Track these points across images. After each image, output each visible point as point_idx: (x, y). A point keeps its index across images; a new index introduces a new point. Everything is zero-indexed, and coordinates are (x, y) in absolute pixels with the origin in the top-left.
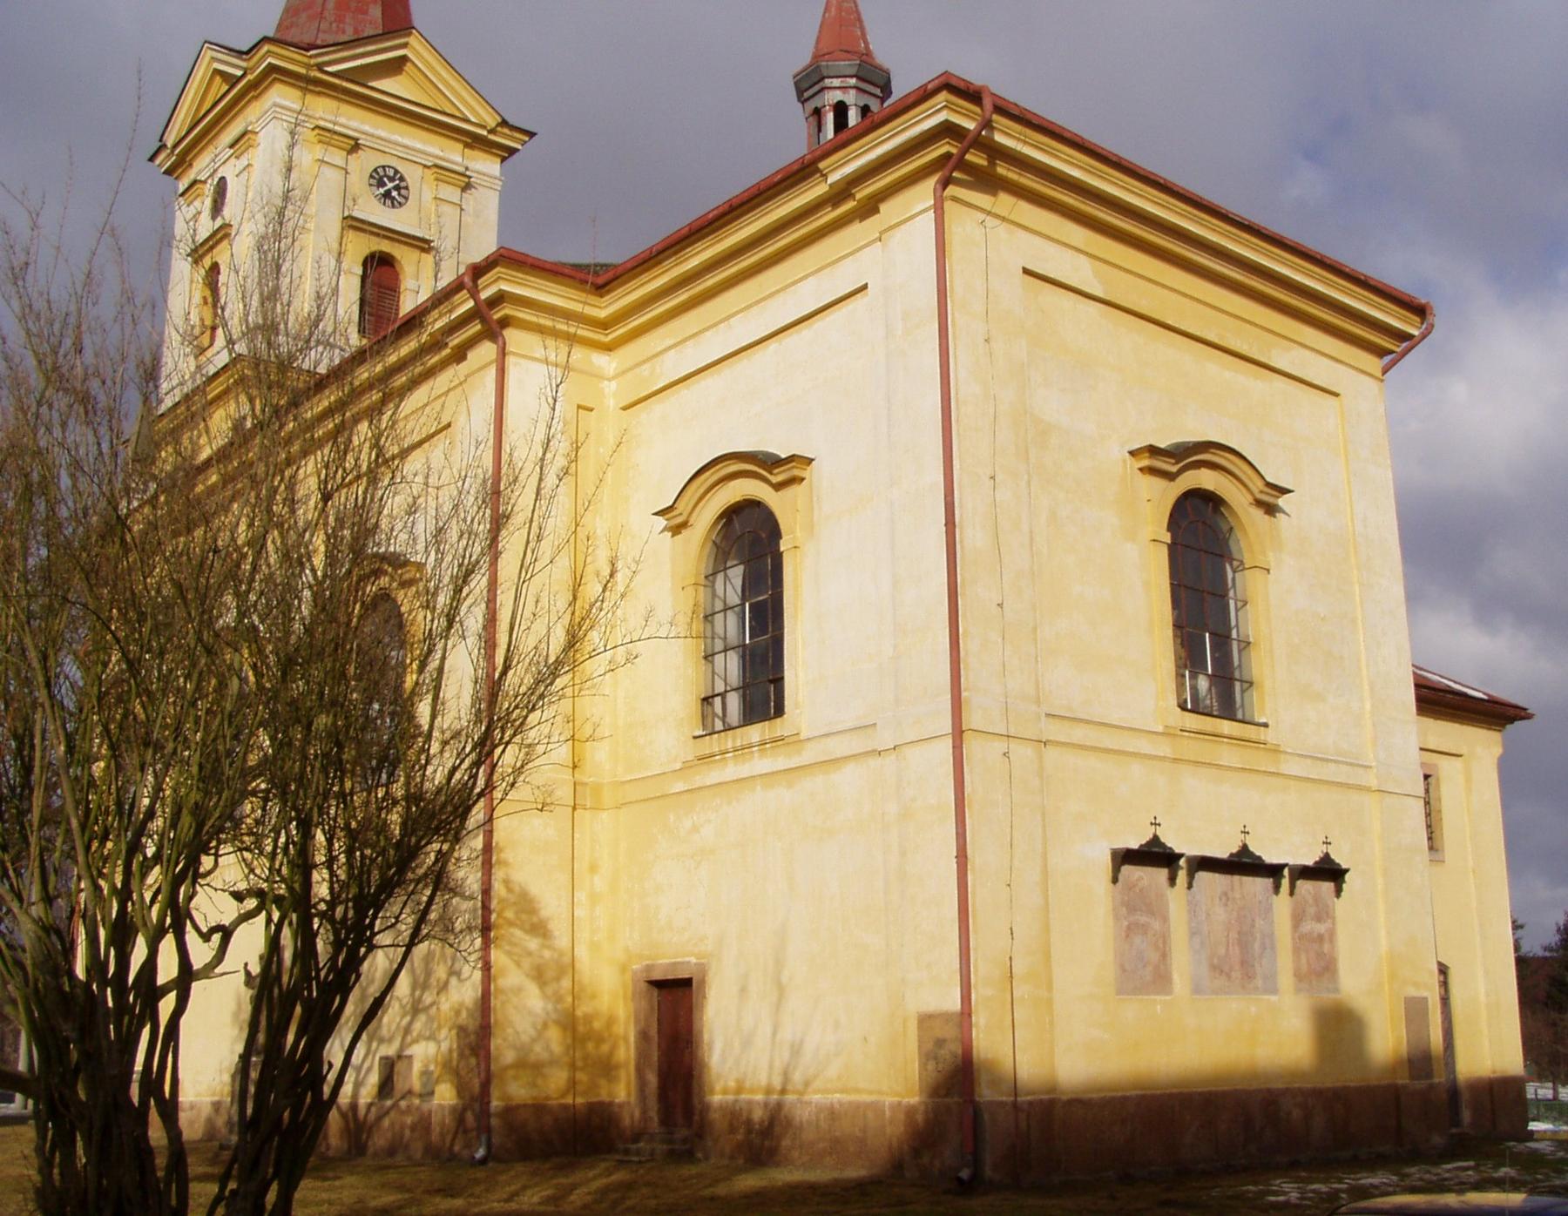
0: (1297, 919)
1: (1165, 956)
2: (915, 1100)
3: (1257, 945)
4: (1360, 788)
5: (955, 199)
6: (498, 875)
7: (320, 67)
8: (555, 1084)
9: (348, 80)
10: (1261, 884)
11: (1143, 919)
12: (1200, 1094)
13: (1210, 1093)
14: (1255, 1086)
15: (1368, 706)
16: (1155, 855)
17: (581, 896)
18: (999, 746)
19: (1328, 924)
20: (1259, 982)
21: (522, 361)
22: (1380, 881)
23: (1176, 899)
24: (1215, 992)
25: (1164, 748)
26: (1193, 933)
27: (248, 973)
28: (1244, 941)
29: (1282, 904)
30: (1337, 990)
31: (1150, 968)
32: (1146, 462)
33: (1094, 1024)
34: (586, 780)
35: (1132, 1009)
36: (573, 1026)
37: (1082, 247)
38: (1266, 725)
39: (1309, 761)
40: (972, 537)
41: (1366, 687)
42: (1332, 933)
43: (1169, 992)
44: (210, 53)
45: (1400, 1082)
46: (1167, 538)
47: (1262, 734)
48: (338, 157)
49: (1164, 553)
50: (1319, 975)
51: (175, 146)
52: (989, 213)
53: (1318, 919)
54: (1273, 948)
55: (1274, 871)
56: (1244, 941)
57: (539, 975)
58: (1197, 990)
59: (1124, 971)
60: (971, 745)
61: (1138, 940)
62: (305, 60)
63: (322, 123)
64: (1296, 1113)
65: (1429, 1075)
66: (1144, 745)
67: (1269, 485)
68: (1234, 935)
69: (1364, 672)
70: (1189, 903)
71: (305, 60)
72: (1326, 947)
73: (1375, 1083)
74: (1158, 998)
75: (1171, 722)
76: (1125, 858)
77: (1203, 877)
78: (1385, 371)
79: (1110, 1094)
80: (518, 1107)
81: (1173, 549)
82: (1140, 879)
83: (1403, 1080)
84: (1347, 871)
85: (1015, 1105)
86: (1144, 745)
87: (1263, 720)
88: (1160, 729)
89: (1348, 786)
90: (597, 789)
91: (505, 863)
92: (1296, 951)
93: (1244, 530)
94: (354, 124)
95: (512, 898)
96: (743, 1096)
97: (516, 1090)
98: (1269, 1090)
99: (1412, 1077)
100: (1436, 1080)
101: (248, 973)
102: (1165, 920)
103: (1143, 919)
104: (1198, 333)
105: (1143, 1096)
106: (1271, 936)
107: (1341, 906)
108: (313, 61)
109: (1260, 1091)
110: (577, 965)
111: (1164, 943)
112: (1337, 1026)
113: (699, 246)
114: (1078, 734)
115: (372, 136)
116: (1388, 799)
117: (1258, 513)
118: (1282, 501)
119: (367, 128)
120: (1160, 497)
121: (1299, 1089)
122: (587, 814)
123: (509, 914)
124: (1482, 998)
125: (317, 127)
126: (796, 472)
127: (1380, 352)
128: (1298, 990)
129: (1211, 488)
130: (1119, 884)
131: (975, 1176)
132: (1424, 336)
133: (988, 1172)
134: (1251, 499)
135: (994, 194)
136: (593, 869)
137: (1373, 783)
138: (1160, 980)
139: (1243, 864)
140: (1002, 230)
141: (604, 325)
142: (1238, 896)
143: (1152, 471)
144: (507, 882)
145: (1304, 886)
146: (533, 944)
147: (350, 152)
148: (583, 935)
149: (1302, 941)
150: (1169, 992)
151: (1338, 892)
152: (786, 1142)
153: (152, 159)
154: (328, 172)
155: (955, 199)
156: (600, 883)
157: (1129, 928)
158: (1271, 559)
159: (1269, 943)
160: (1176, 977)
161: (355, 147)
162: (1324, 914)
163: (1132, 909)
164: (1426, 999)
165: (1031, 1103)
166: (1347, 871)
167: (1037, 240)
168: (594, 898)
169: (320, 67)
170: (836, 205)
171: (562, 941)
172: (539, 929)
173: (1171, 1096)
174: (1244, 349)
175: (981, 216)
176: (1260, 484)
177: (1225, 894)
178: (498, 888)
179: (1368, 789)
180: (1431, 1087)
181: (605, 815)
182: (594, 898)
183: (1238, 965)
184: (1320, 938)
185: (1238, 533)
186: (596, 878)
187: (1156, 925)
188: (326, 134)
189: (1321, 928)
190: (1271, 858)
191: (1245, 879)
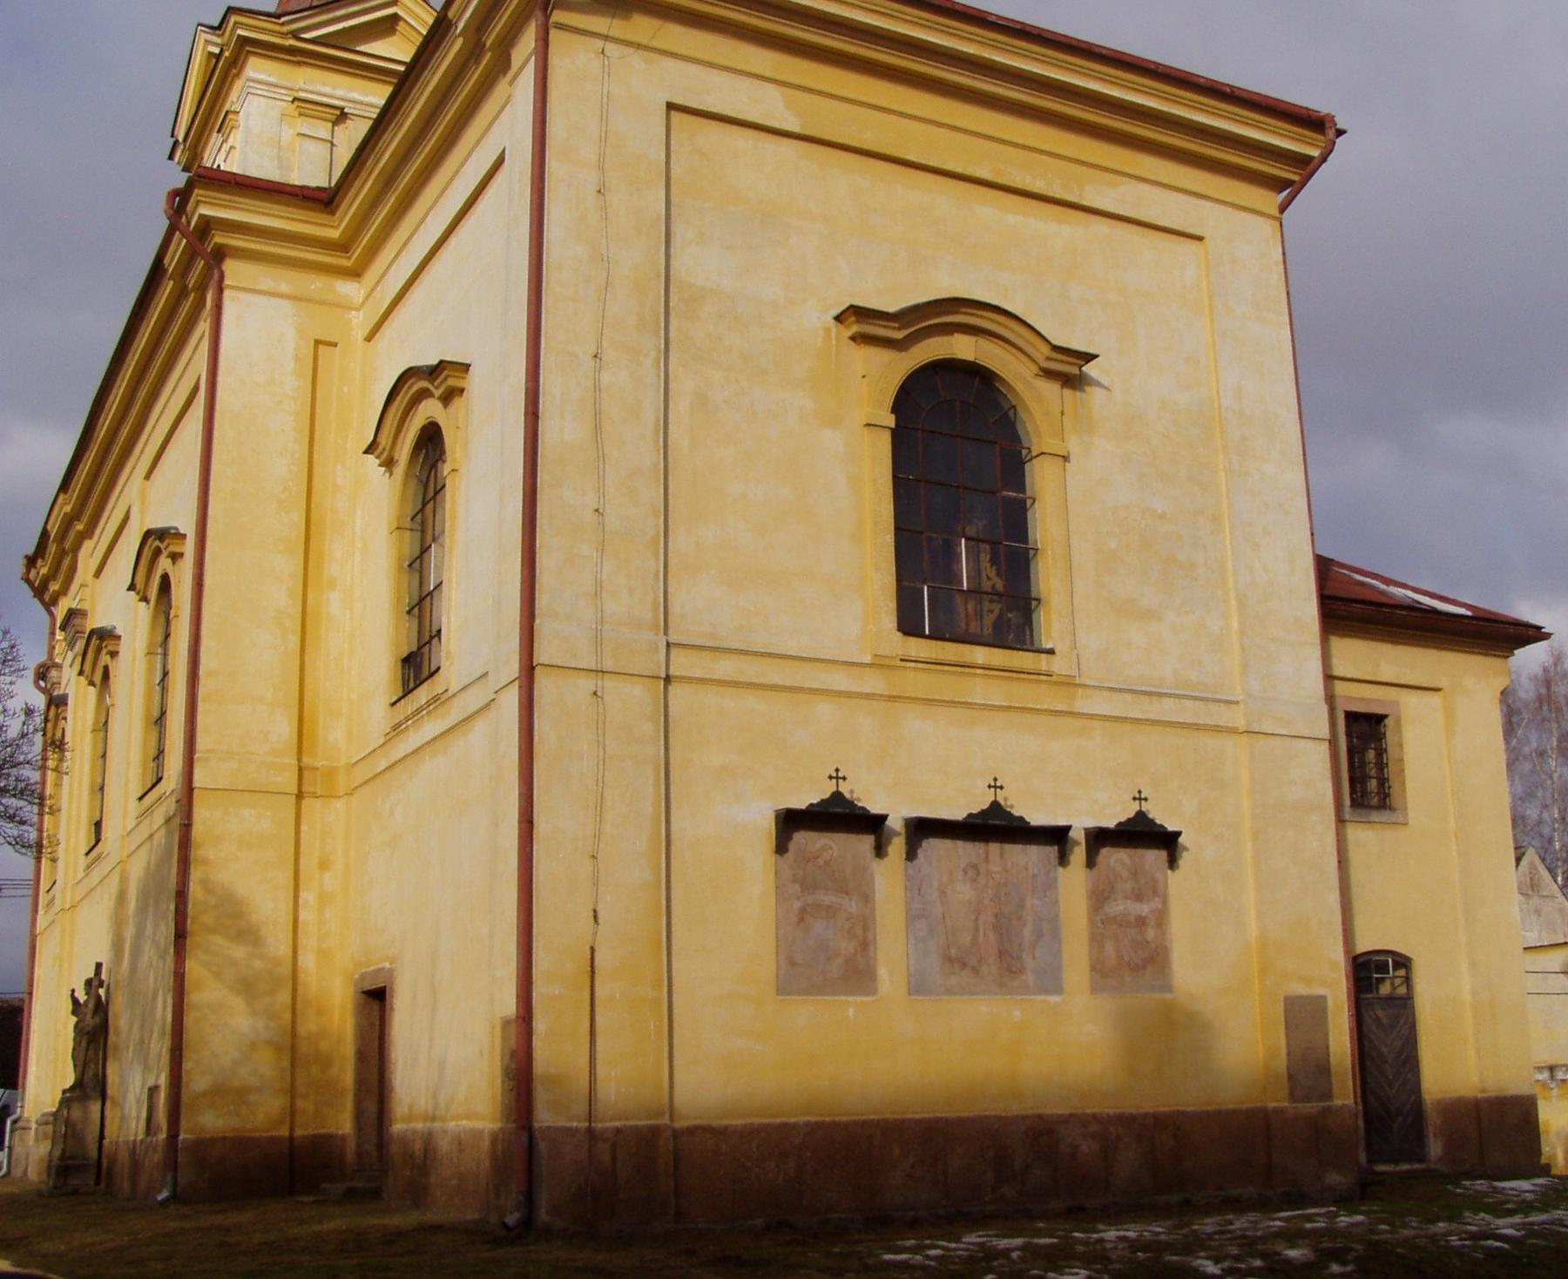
0: (1099, 898)
1: (865, 945)
2: (497, 1125)
3: (1027, 933)
4: (1217, 729)
5: (561, 27)
6: (196, 874)
7: (295, 35)
8: (263, 1115)
9: (327, 46)
10: (1033, 856)
11: (828, 899)
12: (919, 1122)
13: (937, 1120)
14: (1016, 1109)
15: (1235, 624)
16: (839, 815)
17: (307, 896)
18: (587, 684)
19: (1156, 903)
20: (1030, 978)
21: (242, 295)
22: (1248, 847)
23: (888, 877)
24: (949, 992)
25: (874, 683)
26: (913, 917)
27: (75, 1001)
28: (1004, 927)
29: (1074, 881)
30: (1168, 988)
31: (839, 961)
32: (855, 329)
33: (736, 1030)
34: (319, 764)
35: (804, 1014)
36: (293, 1049)
37: (768, 74)
38: (1051, 652)
39: (1128, 697)
40: (557, 429)
41: (1233, 602)
42: (1161, 918)
43: (873, 992)
44: (204, 36)
45: (1272, 1105)
46: (891, 421)
47: (1043, 662)
48: (323, 130)
49: (885, 441)
50: (1137, 969)
51: (185, 140)
52: (606, 38)
53: (1138, 897)
54: (1056, 934)
55: (1057, 836)
56: (1004, 927)
57: (247, 987)
58: (918, 986)
59: (792, 963)
60: (545, 684)
61: (819, 926)
62: (277, 28)
63: (302, 95)
64: (1087, 1147)
65: (1328, 1095)
66: (839, 680)
67: (1056, 349)
68: (987, 918)
69: (1231, 584)
70: (908, 877)
71: (277, 28)
72: (1151, 933)
73: (1231, 1107)
74: (850, 999)
75: (885, 650)
76: (790, 822)
77: (934, 848)
78: (1283, 208)
79: (758, 1121)
80: (213, 1141)
81: (900, 438)
82: (823, 849)
83: (1278, 1100)
84: (1178, 834)
85: (591, 1133)
86: (839, 680)
87: (1049, 646)
88: (868, 659)
89: (1197, 727)
90: (330, 773)
91: (205, 862)
92: (1096, 939)
93: (1027, 409)
94: (340, 93)
95: (212, 901)
96: (437, 1125)
97: (208, 1121)
98: (1040, 1116)
99: (1292, 1097)
100: (1338, 1102)
101: (75, 1001)
102: (867, 898)
103: (828, 899)
104: (959, 170)
105: (820, 1125)
106: (1054, 920)
107: (1177, 882)
108: (285, 29)
109: (1024, 1117)
110: (301, 976)
111: (865, 929)
112: (1168, 1030)
113: (387, 136)
114: (726, 667)
115: (361, 103)
116: (1262, 742)
117: (1050, 389)
118: (1090, 369)
119: (355, 96)
120: (884, 372)
121: (1094, 1116)
122: (319, 802)
123: (208, 919)
124: (1467, 997)
125: (295, 99)
126: (451, 382)
127: (1278, 185)
128: (1095, 989)
129: (970, 357)
130: (790, 856)
131: (528, 1221)
132: (1324, 159)
133: (543, 1215)
134: (1035, 370)
135: (627, 18)
136: (324, 865)
137: (1241, 723)
138: (857, 975)
139: (994, 826)
140: (636, 59)
141: (343, 247)
142: (995, 868)
143: (861, 339)
144: (206, 884)
145: (1115, 858)
146: (239, 952)
147: (335, 123)
148: (308, 943)
149: (1102, 926)
150: (873, 992)
151: (1172, 862)
152: (433, 1180)
153: (171, 157)
154: (311, 146)
155: (561, 27)
156: (330, 881)
157: (803, 910)
158: (1073, 445)
159: (1050, 928)
160: (882, 972)
161: (342, 116)
162: (1149, 890)
163: (808, 886)
164: (1323, 998)
165: (618, 1131)
166: (1178, 834)
167: (693, 69)
168: (324, 899)
169: (295, 35)
170: (477, 62)
171: (278, 945)
172: (248, 934)
173: (865, 1124)
174: (1039, 186)
175: (600, 43)
176: (1045, 350)
177: (975, 867)
178: (195, 890)
179: (1233, 731)
180: (1328, 1110)
181: (339, 805)
182: (324, 899)
183: (1000, 955)
184: (1141, 922)
185: (1022, 414)
186: (327, 876)
187: (852, 906)
188: (304, 105)
189: (1144, 909)
190: (1037, 819)
191: (1008, 847)
